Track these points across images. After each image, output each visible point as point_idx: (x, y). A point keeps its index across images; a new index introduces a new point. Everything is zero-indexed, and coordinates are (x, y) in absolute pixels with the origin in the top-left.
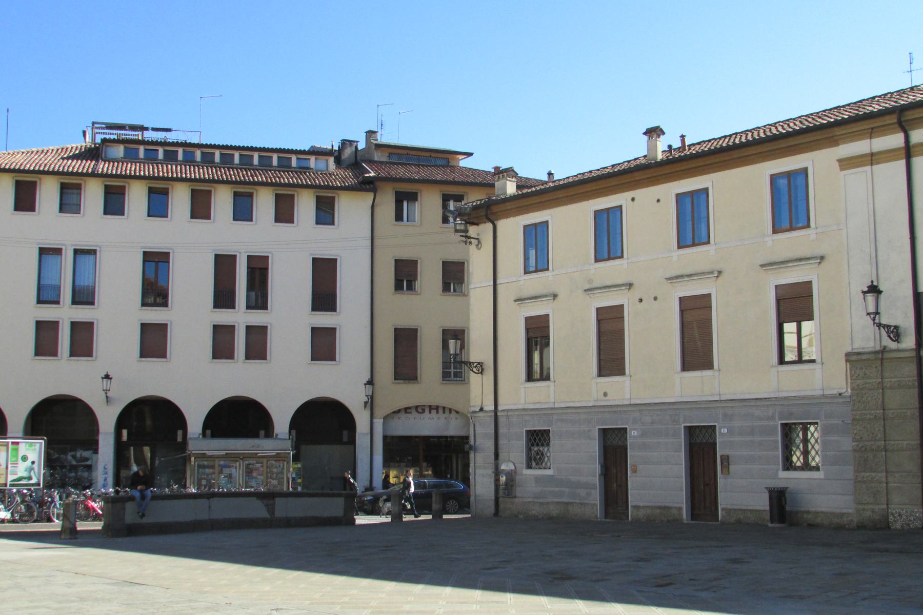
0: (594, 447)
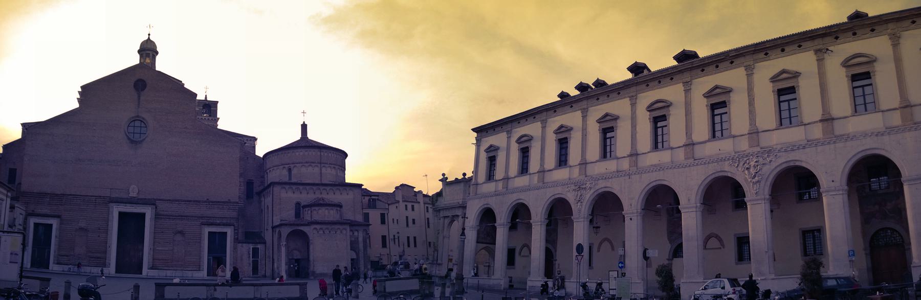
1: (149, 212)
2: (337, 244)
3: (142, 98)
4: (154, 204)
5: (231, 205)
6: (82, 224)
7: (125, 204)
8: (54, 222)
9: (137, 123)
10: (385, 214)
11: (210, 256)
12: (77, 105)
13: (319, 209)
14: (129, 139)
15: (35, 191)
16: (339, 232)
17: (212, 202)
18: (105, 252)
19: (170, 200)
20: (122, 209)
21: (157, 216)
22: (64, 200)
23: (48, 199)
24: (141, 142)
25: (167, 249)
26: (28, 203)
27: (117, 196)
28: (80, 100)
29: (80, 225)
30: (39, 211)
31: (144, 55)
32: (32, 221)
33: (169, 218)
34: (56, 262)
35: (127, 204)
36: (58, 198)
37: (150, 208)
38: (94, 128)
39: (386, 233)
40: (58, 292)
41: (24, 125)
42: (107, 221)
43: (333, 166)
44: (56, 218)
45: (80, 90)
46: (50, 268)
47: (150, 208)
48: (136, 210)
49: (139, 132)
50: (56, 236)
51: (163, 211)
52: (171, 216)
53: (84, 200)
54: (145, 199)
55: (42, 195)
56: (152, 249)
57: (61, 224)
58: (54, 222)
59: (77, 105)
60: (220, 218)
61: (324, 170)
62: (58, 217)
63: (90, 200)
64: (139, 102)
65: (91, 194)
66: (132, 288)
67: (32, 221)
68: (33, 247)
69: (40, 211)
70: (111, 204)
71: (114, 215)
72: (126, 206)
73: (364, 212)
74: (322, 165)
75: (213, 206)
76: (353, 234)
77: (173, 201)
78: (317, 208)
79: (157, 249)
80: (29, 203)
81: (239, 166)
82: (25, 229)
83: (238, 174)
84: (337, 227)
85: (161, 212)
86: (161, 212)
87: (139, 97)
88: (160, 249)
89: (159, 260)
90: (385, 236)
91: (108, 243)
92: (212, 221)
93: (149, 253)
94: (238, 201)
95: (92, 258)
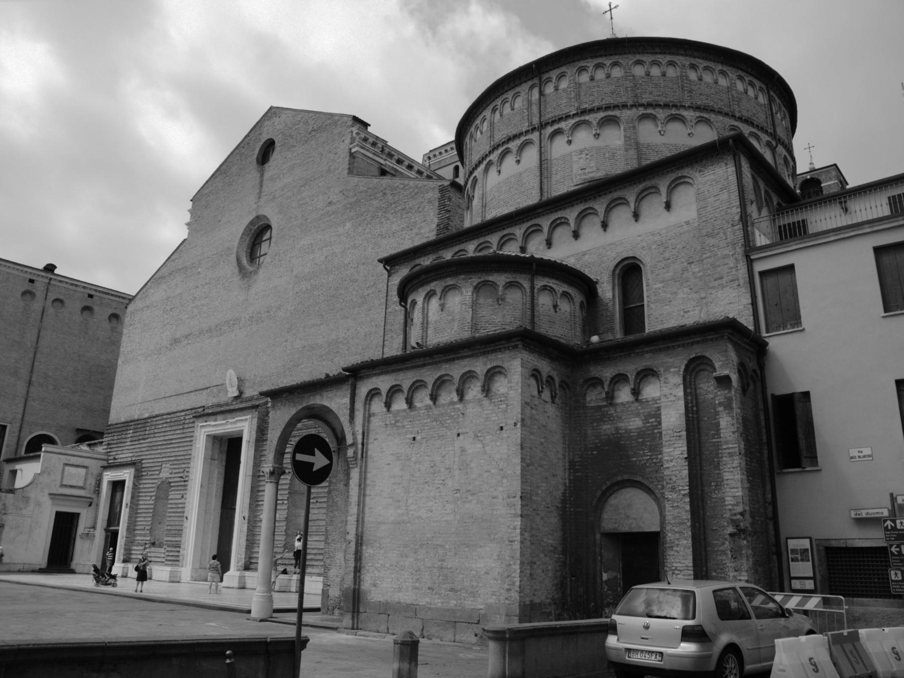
0: (888, 498)
2: (463, 450)
3: (267, 175)
8: (127, 475)
16: (474, 391)
43: (601, 115)
50: (127, 504)
54: (219, 405)
56: (246, 518)
61: (559, 147)
62: (132, 464)
72: (216, 420)
73: (759, 267)
74: (550, 130)
76: (636, 392)
84: (456, 370)
87: (262, 175)
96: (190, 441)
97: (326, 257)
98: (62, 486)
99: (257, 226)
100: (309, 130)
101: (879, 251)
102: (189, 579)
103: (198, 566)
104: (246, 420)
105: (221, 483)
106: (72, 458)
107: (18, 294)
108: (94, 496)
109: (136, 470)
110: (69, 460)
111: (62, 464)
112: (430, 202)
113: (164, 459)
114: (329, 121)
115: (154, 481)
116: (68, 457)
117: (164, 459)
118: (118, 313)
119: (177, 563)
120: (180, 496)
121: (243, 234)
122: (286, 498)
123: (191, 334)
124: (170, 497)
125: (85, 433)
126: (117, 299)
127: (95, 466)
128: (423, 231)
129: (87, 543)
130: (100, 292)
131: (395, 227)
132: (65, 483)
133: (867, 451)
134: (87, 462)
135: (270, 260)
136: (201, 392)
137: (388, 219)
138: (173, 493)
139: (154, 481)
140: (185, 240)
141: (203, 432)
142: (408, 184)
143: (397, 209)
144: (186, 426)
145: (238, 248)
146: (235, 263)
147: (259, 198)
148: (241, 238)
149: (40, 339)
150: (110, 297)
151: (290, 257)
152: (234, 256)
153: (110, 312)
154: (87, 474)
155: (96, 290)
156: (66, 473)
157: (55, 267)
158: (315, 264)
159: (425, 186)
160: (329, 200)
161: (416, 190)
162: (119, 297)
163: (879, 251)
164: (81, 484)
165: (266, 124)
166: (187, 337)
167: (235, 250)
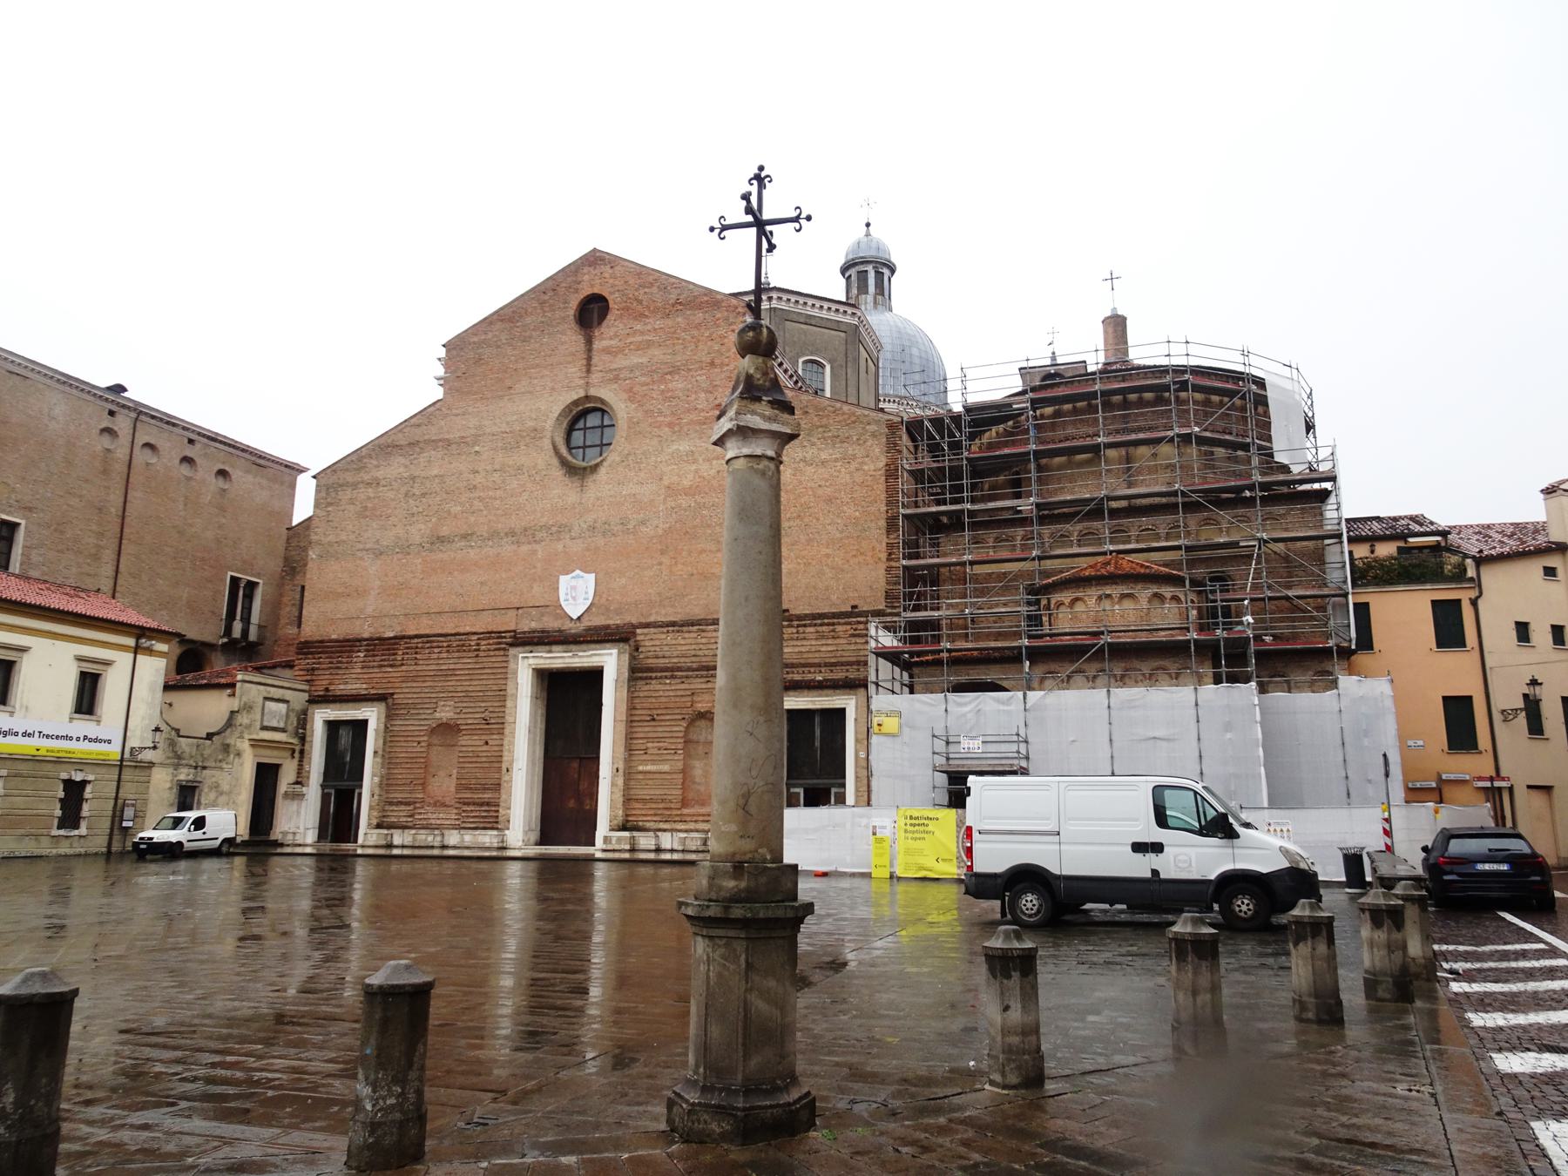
1: (610, 661)
3: (597, 345)
4: (625, 640)
5: (642, 333)
6: (445, 713)
7: (547, 648)
8: (372, 715)
9: (593, 420)
10: (1458, 602)
11: (795, 786)
12: (438, 393)
13: (1077, 599)
14: (564, 463)
15: (334, 637)
17: (800, 618)
18: (497, 787)
19: (673, 624)
20: (542, 661)
21: (637, 673)
22: (400, 652)
23: (362, 655)
24: (594, 468)
25: (666, 768)
26: (313, 669)
27: (534, 625)
28: (444, 382)
29: (437, 715)
30: (340, 688)
31: (854, 278)
32: (321, 716)
33: (673, 677)
34: (375, 822)
35: (554, 648)
36: (383, 647)
37: (615, 651)
38: (477, 448)
39: (1468, 685)
40: (1085, 362)
41: (1445, 699)
42: (501, 697)
44: (375, 704)
45: (441, 371)
46: (360, 841)
47: (615, 651)
48: (576, 660)
49: (599, 442)
50: (375, 752)
51: (657, 657)
52: (679, 669)
53: (448, 646)
55: (348, 645)
56: (621, 771)
57: (389, 717)
58: (372, 715)
59: (438, 393)
60: (826, 665)
63: (463, 645)
64: (589, 359)
65: (468, 629)
66: (430, 1058)
67: (321, 716)
68: (323, 786)
69: (342, 687)
70: (512, 651)
71: (519, 681)
72: (550, 652)
75: (801, 629)
77: (682, 626)
78: (1065, 596)
79: (640, 768)
80: (318, 669)
81: (883, 496)
82: (303, 739)
83: (883, 523)
85: (650, 661)
86: (650, 661)
87: (589, 342)
88: (649, 768)
89: (644, 801)
90: (1467, 701)
91: (505, 759)
92: (797, 677)
93: (613, 784)
94: (882, 607)
95: (468, 804)
96: (504, 674)
97: (718, 472)
98: (264, 728)
99: (581, 408)
100: (671, 301)
101: (1434, 602)
102: (520, 843)
103: (527, 828)
104: (611, 654)
105: (543, 726)
106: (272, 689)
107: (96, 432)
108: (295, 741)
109: (388, 708)
110: (269, 692)
111: (262, 699)
112: (874, 435)
113: (442, 695)
114: (706, 299)
115: (426, 722)
116: (269, 688)
117: (442, 695)
118: (227, 469)
119: (495, 825)
120: (482, 743)
121: (560, 415)
122: (680, 746)
123: (472, 534)
124: (460, 743)
125: (191, 646)
126: (226, 448)
127: (299, 700)
128: (866, 468)
129: (294, 806)
130: (204, 436)
131: (824, 456)
132: (265, 724)
133: (1420, 743)
134: (288, 695)
135: (618, 459)
136: (503, 612)
137: (813, 444)
138: (465, 737)
139: (426, 722)
140: (439, 401)
141: (524, 668)
142: (841, 409)
143: (826, 435)
144: (482, 654)
145: (552, 432)
146: (552, 452)
147: (588, 371)
148: (557, 419)
149: (128, 504)
150: (217, 445)
151: (656, 462)
152: (547, 443)
153: (222, 467)
154: (288, 707)
155: (199, 434)
156: (266, 711)
157: (125, 390)
158: (700, 477)
159: (865, 416)
160: (717, 402)
161: (853, 419)
162: (230, 445)
163: (1434, 602)
164: (282, 725)
165: (585, 271)
166: (465, 537)
167: (549, 435)
